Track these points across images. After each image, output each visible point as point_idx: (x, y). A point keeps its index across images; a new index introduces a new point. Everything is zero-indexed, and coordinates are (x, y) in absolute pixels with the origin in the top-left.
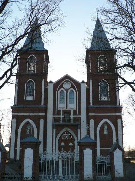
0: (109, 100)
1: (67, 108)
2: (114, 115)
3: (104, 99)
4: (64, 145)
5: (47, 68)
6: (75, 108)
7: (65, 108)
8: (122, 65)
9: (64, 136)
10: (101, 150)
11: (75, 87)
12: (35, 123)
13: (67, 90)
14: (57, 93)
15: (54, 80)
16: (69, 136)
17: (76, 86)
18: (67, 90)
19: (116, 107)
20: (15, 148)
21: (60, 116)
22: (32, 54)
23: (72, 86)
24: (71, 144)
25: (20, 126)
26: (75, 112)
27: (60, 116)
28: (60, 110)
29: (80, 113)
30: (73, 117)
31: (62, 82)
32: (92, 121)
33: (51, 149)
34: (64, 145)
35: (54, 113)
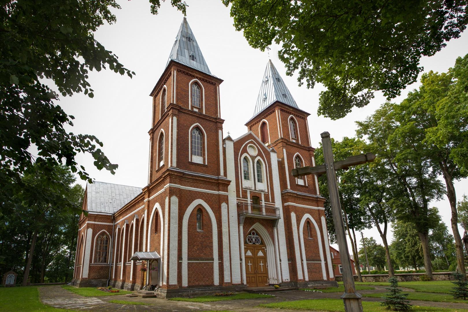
0: (206, 164)
2: (213, 195)
3: (197, 159)
5: (452, 185)
6: (266, 191)
7: (253, 189)
9: (250, 237)
10: (308, 264)
13: (253, 158)
14: (240, 159)
15: (235, 137)
16: (257, 238)
19: (218, 180)
20: (178, 261)
21: (247, 201)
22: (197, 78)
23: (260, 154)
24: (260, 254)
26: (267, 199)
28: (246, 191)
29: (273, 201)
33: (239, 262)
35: (238, 196)
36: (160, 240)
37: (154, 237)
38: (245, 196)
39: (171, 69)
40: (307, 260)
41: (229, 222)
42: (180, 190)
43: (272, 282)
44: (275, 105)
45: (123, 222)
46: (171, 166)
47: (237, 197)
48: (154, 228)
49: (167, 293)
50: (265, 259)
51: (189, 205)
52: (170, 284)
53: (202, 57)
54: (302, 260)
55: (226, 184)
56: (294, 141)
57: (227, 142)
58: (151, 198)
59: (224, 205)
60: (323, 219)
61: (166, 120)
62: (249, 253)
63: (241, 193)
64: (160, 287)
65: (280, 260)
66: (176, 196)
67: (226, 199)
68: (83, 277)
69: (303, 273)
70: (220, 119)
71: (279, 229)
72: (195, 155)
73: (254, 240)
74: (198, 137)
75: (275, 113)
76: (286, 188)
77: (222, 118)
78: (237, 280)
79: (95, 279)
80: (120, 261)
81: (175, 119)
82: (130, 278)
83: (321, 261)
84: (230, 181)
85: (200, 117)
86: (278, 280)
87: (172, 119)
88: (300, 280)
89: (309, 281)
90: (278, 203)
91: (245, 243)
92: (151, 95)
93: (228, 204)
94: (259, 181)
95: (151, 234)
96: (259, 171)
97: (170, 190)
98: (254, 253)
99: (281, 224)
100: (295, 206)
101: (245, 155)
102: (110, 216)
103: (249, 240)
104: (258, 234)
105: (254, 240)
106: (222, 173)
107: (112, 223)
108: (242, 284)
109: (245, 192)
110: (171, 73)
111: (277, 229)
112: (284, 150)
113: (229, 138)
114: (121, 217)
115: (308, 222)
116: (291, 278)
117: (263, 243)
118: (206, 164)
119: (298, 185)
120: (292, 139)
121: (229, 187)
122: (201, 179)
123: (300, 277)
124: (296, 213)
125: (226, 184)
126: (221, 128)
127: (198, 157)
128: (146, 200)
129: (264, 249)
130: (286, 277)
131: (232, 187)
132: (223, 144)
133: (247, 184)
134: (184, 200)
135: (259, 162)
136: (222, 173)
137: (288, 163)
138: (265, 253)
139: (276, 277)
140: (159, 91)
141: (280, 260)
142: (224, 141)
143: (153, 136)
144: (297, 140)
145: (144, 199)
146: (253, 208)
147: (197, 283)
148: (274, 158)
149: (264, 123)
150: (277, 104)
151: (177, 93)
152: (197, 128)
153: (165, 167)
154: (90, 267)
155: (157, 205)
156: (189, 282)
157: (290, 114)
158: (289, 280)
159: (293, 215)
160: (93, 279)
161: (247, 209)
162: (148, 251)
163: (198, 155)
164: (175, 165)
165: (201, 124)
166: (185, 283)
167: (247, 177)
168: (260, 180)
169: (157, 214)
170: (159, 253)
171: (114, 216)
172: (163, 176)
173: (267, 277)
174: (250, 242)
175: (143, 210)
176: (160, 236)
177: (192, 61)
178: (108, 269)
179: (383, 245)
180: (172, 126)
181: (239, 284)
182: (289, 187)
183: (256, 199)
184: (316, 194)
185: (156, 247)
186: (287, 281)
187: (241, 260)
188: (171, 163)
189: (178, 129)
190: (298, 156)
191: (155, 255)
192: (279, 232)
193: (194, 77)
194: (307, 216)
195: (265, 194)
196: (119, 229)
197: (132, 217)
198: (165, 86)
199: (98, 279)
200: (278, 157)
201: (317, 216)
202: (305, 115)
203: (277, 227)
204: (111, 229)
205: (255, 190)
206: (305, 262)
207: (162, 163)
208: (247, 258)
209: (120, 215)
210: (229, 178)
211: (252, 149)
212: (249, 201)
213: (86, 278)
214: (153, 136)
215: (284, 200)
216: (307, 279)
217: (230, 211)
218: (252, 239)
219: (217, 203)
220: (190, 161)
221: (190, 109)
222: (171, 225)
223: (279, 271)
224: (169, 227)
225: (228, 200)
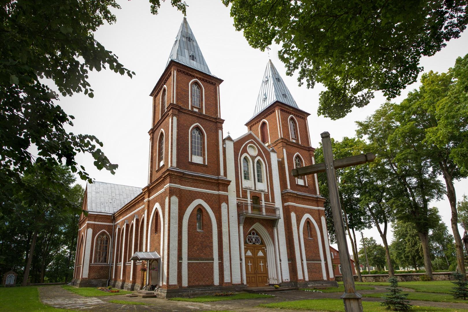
0: (206, 164)
3: (197, 159)
6: (266, 191)
7: (253, 189)
8: (440, 303)
9: (250, 237)
10: (308, 264)
12: (212, 208)
13: (253, 158)
15: (235, 137)
20: (178, 261)
21: (247, 201)
22: (197, 78)
23: (260, 154)
24: (260, 254)
26: (267, 199)
28: (246, 191)
29: (273, 201)
31: (246, 143)
33: (239, 262)
35: (238, 196)
37: (154, 237)
38: (245, 196)
39: (171, 69)
40: (307, 260)
42: (180, 190)
44: (275, 105)
45: (123, 222)
46: (171, 166)
47: (237, 197)
48: (154, 228)
49: (167, 293)
50: (264, 259)
51: (189, 205)
54: (302, 260)
55: (226, 184)
56: (294, 141)
58: (151, 198)
59: (224, 205)
60: (323, 219)
61: (166, 120)
62: (249, 253)
63: (241, 193)
64: (160, 287)
65: (280, 260)
66: (176, 196)
67: (226, 199)
68: (83, 277)
69: (303, 273)
70: (220, 119)
71: (279, 229)
72: (195, 155)
73: (254, 240)
75: (275, 114)
76: (286, 188)
77: (222, 118)
78: (237, 280)
79: (95, 279)
81: (175, 119)
83: (321, 261)
84: (230, 181)
85: (200, 117)
86: (278, 280)
87: (172, 119)
88: (300, 280)
89: (309, 281)
90: (278, 203)
91: (245, 243)
92: (151, 95)
93: (228, 204)
95: (151, 234)
96: (259, 171)
97: (170, 190)
98: (254, 253)
99: (281, 224)
100: (295, 206)
101: (245, 155)
102: (109, 216)
104: (258, 234)
105: (254, 240)
106: (222, 173)
107: (112, 223)
108: (242, 284)
109: (245, 192)
110: (171, 73)
111: (277, 229)
112: (284, 150)
113: (229, 138)
114: (121, 217)
115: (308, 222)
117: (263, 243)
118: (206, 164)
119: (298, 185)
120: (292, 139)
121: (229, 187)
122: (201, 179)
123: (300, 277)
124: (296, 213)
125: (226, 184)
126: (221, 128)
127: (198, 157)
128: (146, 200)
129: (264, 249)
130: (286, 277)
131: (232, 187)
132: (223, 144)
133: (247, 184)
134: (184, 200)
135: (259, 162)
136: (222, 173)
137: (288, 163)
138: (265, 253)
139: (276, 277)
140: (159, 91)
141: (280, 260)
142: (224, 141)
143: (153, 136)
144: (297, 140)
145: (144, 199)
146: (253, 208)
147: (197, 283)
148: (274, 158)
149: (264, 123)
150: (277, 104)
152: (197, 128)
153: (165, 167)
154: (90, 267)
155: (157, 205)
156: (189, 282)
157: (290, 114)
158: (289, 280)
159: (293, 215)
161: (247, 209)
162: (148, 251)
163: (198, 155)
164: (175, 165)
166: (185, 283)
167: (247, 177)
168: (260, 180)
169: (157, 214)
170: (159, 253)
171: (114, 217)
173: (267, 277)
174: (250, 242)
176: (160, 236)
177: (192, 61)
178: (108, 269)
180: (172, 126)
181: (239, 284)
182: (289, 187)
183: (256, 199)
184: (316, 194)
185: (156, 247)
186: (287, 281)
187: (241, 260)
188: (171, 163)
190: (298, 156)
191: (155, 255)
192: (279, 232)
193: (194, 77)
194: (307, 216)
195: (265, 194)
196: (119, 229)
197: (132, 217)
198: (165, 86)
199: (98, 279)
200: (278, 157)
201: (317, 216)
202: (305, 115)
203: (277, 227)
204: (111, 229)
205: (255, 190)
206: (305, 262)
207: (162, 164)
208: (247, 258)
209: (120, 215)
210: (276, 206)
212: (249, 201)
214: (153, 136)
215: (284, 200)
216: (307, 279)
217: (230, 211)
218: (252, 239)
219: (217, 203)
221: (190, 109)
222: (171, 225)
223: (279, 271)
224: (169, 227)
225: (228, 200)
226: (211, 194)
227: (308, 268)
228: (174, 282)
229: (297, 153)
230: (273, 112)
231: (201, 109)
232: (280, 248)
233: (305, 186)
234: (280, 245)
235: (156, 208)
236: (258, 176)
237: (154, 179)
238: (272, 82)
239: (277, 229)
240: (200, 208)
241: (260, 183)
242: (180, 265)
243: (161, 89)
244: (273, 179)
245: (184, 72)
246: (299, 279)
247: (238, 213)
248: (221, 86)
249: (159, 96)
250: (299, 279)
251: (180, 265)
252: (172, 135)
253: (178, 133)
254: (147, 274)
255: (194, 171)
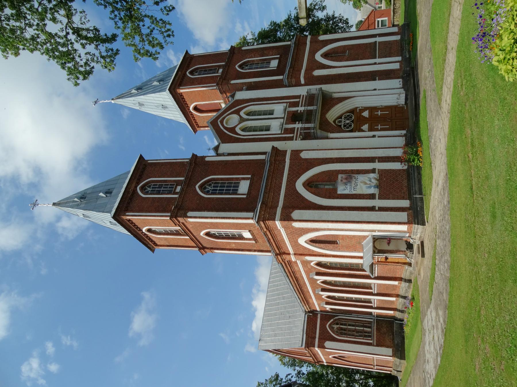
0: (250, 176)
1: (283, 118)
3: (244, 187)
4: (362, 114)
6: (285, 104)
7: (282, 120)
9: (345, 126)
11: (238, 109)
13: (242, 120)
16: (345, 118)
17: (235, 107)
18: (242, 120)
20: (377, 211)
22: (136, 187)
23: (237, 112)
24: (366, 114)
25: (321, 61)
26: (296, 104)
27: (303, 96)
29: (298, 97)
30: (304, 106)
32: (317, 73)
34: (362, 114)
35: (291, 139)
36: (348, 236)
37: (342, 246)
38: (292, 131)
39: (123, 220)
40: (375, 58)
41: (325, 150)
42: (284, 208)
43: (402, 101)
44: (173, 92)
45: (319, 298)
46: (252, 218)
47: (292, 140)
48: (331, 246)
49: (418, 224)
50: (372, 109)
51: (303, 198)
52: (406, 221)
53: (107, 181)
54: (375, 64)
55: (277, 154)
56: (221, 71)
57: (220, 151)
58: (291, 251)
59: (304, 155)
60: (322, 38)
61: (190, 227)
62: (365, 127)
63: (287, 134)
64: (410, 236)
65: (375, 90)
66: (291, 213)
67: (296, 153)
68: (391, 354)
69: (393, 63)
70: (191, 160)
71: (334, 91)
72: (237, 190)
73: (348, 122)
74: (214, 187)
75: (184, 92)
76: (281, 80)
77: (190, 156)
78: (402, 141)
79: (393, 339)
80: (369, 302)
81: (190, 214)
82: (393, 285)
83: (376, 42)
84: (273, 147)
85: (189, 184)
86: (399, 94)
87: (191, 217)
88: (400, 66)
89: (402, 56)
90: (302, 91)
91: (351, 131)
92: (153, 250)
93: (302, 151)
94: (272, 114)
95: (339, 250)
96: (259, 113)
97: (284, 220)
98: (365, 120)
99: (326, 88)
100: (306, 70)
101: (238, 130)
102: (308, 318)
103: (348, 128)
104: (340, 117)
105: (348, 122)
106: (262, 157)
107: (317, 314)
108: (405, 135)
109: (287, 131)
110: (129, 220)
111: (335, 93)
112: (233, 82)
113: (216, 149)
114: (310, 301)
115: (325, 56)
116: (398, 78)
117: (352, 111)
118: (250, 176)
119: (278, 66)
120: (217, 73)
121: (280, 148)
122: (270, 181)
123: (397, 66)
124: (314, 70)
125: (277, 154)
126: (203, 157)
127: (240, 187)
128: (293, 258)
129: (360, 110)
130: (397, 83)
131: (280, 145)
132: (224, 156)
133: (275, 126)
134: (296, 203)
135: (248, 114)
136: (262, 157)
137: (249, 78)
138: (365, 109)
139: (397, 96)
140: (150, 239)
141: (375, 90)
142: (218, 155)
143: (208, 248)
144: (219, 67)
145: (290, 262)
146: (308, 121)
147: (405, 189)
148: (240, 95)
149: (196, 108)
150: (173, 91)
151: (156, 212)
152: (202, 187)
153: (252, 228)
154: (377, 345)
155: (302, 241)
156: (403, 198)
157: (185, 74)
158: (401, 80)
159: (317, 73)
160: (394, 342)
161: (309, 128)
162: (361, 254)
163: (238, 187)
164: (251, 214)
165: (198, 183)
166: (406, 203)
167: (268, 128)
168: (271, 113)
169: (313, 241)
170: (365, 237)
171: (309, 312)
172: (265, 230)
173: (396, 107)
174: (351, 126)
175: (306, 264)
176: (343, 237)
177: (113, 194)
178: (381, 320)
179: (178, 218)
180: (200, 217)
181: (406, 139)
182: (281, 77)
183: (294, 117)
184: (290, 45)
185: (355, 243)
186: (401, 83)
187: (374, 136)
188: (248, 218)
189: (204, 211)
190: (241, 66)
191: (368, 244)
192: (338, 91)
193: (135, 191)
194: (318, 57)
195: (289, 107)
196: (328, 303)
197: (313, 282)
198: (144, 230)
199: (393, 335)
200: (241, 90)
201: (317, 45)
202: (187, 56)
203: (332, 93)
204: (326, 316)
205: (283, 118)
206: (378, 60)
207: (247, 235)
208: (371, 129)
209: (308, 303)
210: (305, 94)
211: (230, 121)
212: (298, 125)
213: (393, 351)
214: (208, 248)
215: (298, 84)
216: (399, 58)
217: (311, 149)
218: (348, 124)
219: (301, 165)
220: (245, 196)
221: (176, 196)
222: (330, 219)
223: (389, 94)
224: (332, 222)
225: (297, 151)
226: (289, 170)
227: (386, 57)
228: (403, 216)
229: (237, 67)
230: (182, 95)
231: (178, 183)
232: (359, 89)
233: (279, 59)
234: (354, 90)
235: (306, 242)
236: (264, 114)
237: (267, 246)
238: (142, 97)
239: (335, 93)
240: (308, 184)
241: (275, 113)
242: (381, 209)
243: (147, 236)
244: (269, 96)
245: (129, 203)
246: (399, 68)
247: (313, 139)
248: (146, 158)
249: (154, 239)
250: (399, 68)
251: (381, 209)
252: (211, 218)
253: (209, 210)
254: (392, 257)
255: (259, 191)
